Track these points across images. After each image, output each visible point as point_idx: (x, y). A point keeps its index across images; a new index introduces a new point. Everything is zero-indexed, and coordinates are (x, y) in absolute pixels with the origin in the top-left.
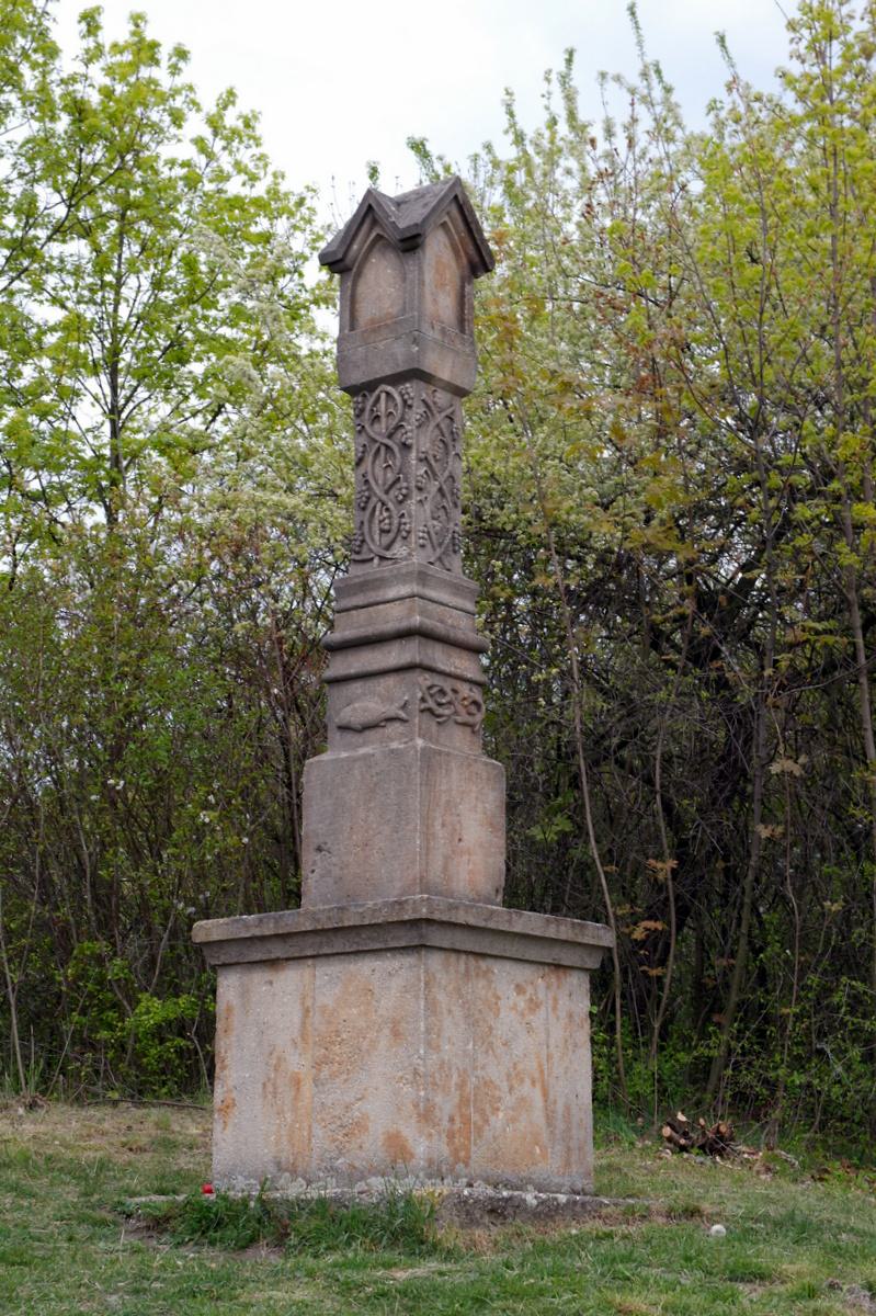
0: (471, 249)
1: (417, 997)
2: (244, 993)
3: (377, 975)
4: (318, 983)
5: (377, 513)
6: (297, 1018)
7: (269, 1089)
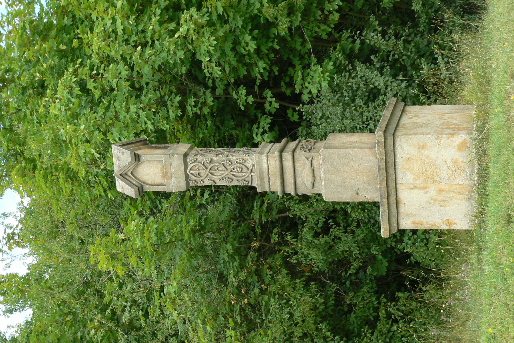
0: (139, 144)
1: (411, 138)
2: (408, 215)
3: (403, 156)
4: (405, 182)
5: (235, 173)
6: (417, 191)
7: (442, 204)
